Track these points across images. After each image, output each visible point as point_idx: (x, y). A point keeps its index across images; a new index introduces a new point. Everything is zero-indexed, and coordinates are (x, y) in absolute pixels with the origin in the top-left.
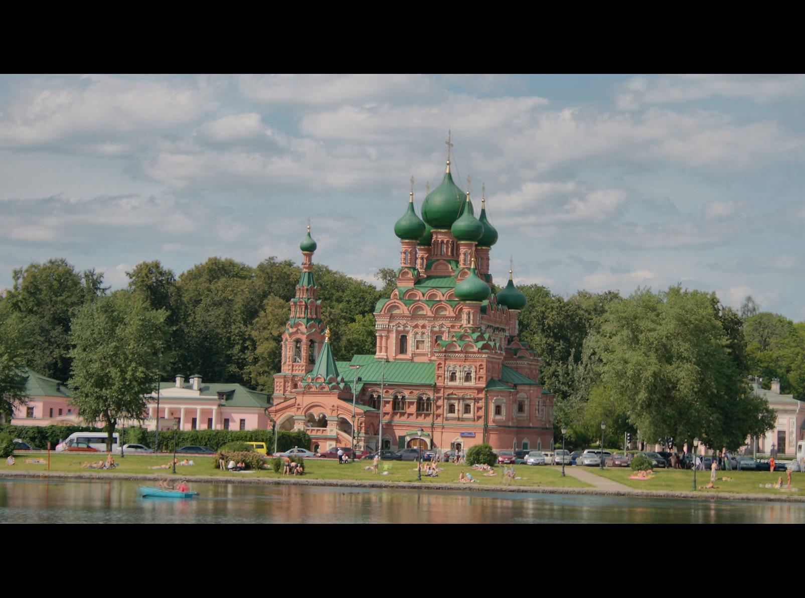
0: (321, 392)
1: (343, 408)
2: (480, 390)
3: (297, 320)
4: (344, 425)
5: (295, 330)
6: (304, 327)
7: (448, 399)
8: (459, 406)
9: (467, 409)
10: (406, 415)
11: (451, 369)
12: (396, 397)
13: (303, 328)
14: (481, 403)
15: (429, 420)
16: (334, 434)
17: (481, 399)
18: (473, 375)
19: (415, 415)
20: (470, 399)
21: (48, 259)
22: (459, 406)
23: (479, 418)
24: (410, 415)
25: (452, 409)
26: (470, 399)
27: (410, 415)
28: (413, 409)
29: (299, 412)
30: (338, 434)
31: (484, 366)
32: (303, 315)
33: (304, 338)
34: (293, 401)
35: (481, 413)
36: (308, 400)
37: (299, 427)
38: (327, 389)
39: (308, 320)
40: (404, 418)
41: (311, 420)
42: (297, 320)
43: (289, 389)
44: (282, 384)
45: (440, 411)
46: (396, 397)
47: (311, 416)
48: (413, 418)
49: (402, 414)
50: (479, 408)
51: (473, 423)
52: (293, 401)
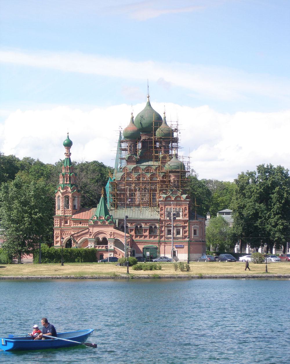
0: (104, 225)
1: (117, 234)
2: (185, 222)
3: (65, 185)
4: (117, 243)
5: (65, 191)
6: (69, 189)
7: (167, 227)
8: (174, 231)
9: (178, 233)
10: (143, 237)
11: (169, 210)
12: (137, 227)
13: (69, 190)
14: (187, 229)
15: (157, 239)
16: (112, 248)
17: (186, 226)
18: (181, 214)
19: (148, 237)
20: (180, 227)
21: (254, 170)
22: (174, 231)
23: (185, 237)
24: (146, 236)
25: (169, 232)
26: (180, 227)
27: (146, 236)
28: (147, 233)
29: (91, 237)
30: (114, 248)
31: (187, 208)
32: (68, 182)
33: (70, 195)
34: (87, 230)
35: (187, 234)
36: (96, 230)
37: (91, 246)
38: (107, 223)
39: (72, 185)
40: (142, 239)
41: (98, 242)
42: (65, 185)
43: (63, 224)
44: (59, 221)
45: (163, 234)
46: (137, 227)
47: (98, 239)
48: (147, 239)
49: (141, 236)
50: (185, 232)
51: (182, 240)
52: (87, 230)
